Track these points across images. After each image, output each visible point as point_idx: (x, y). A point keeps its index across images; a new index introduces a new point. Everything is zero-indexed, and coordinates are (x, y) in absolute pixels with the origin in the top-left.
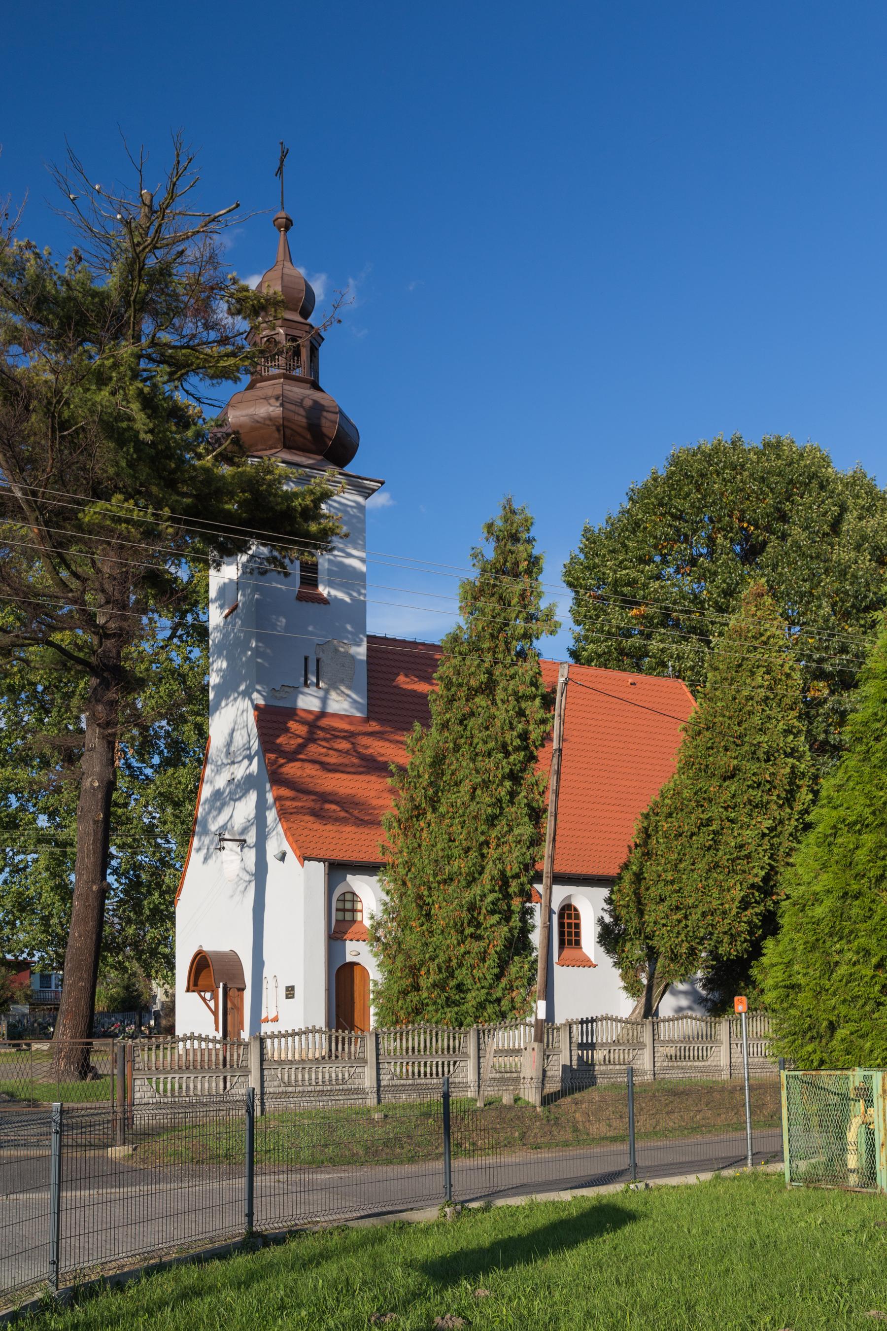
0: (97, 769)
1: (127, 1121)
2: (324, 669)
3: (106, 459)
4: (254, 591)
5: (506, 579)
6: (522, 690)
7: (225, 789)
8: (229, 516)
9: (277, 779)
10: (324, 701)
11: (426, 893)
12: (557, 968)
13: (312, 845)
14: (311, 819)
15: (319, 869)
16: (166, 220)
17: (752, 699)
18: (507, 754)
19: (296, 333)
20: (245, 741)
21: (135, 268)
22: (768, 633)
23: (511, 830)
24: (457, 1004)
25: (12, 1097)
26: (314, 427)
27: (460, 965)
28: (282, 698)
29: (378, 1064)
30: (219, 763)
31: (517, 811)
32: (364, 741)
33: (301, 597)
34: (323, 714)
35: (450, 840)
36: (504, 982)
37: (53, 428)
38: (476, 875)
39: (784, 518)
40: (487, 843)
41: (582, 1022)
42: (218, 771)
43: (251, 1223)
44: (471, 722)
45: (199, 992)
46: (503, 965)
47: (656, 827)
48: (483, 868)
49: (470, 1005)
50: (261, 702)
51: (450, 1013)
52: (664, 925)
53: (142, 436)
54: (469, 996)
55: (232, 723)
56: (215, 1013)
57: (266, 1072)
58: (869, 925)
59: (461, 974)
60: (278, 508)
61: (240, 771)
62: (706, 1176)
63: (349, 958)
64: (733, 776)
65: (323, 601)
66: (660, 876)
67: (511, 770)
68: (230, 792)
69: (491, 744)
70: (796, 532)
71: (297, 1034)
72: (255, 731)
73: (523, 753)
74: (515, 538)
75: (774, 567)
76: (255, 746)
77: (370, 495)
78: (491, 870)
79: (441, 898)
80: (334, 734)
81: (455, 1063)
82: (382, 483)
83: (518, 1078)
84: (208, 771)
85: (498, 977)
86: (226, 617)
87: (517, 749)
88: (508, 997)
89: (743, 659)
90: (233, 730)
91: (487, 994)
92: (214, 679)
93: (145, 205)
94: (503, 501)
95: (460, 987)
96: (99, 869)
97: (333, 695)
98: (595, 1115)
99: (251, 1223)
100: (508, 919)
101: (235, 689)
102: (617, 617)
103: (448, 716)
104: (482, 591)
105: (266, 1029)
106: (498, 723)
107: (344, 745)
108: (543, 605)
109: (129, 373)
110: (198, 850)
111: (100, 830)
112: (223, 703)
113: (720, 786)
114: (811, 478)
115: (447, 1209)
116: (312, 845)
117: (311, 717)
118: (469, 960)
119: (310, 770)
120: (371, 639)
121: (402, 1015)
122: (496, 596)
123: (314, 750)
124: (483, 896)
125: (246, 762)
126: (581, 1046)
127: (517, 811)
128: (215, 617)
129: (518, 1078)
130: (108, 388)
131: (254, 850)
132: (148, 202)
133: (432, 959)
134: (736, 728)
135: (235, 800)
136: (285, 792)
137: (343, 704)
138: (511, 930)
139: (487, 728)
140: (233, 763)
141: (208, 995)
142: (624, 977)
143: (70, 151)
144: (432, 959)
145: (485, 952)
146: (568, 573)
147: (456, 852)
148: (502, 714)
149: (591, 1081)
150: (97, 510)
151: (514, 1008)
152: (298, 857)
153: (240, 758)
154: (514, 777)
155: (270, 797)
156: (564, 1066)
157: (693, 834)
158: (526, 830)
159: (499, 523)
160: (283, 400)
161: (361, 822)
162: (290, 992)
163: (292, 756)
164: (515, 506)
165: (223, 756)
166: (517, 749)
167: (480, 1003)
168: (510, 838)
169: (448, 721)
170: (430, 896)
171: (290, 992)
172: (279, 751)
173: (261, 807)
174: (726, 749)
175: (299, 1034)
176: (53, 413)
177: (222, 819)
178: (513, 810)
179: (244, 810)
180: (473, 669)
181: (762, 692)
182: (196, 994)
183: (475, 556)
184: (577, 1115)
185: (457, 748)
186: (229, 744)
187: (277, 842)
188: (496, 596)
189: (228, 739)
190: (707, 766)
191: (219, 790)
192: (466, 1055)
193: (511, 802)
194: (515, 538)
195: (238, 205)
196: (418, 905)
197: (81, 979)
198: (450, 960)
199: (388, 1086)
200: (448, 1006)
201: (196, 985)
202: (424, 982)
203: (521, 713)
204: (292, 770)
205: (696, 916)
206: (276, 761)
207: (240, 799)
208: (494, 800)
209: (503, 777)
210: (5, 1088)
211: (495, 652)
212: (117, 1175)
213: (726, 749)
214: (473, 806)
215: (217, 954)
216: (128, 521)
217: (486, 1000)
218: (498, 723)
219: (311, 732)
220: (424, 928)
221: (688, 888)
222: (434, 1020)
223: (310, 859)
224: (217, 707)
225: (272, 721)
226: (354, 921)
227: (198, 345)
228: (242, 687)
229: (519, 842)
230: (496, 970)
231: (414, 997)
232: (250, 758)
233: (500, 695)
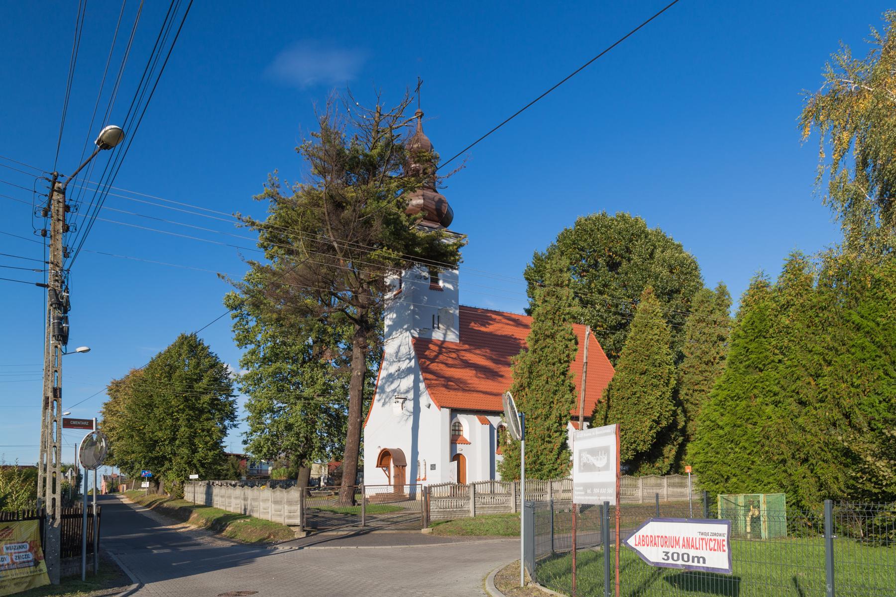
4: (413, 284)
8: (417, 254)
9: (425, 370)
10: (445, 335)
12: (496, 455)
15: (446, 412)
24: (539, 470)
26: (439, 211)
32: (463, 353)
33: (432, 288)
34: (444, 342)
36: (559, 461)
39: (628, 250)
40: (553, 402)
42: (391, 363)
46: (559, 454)
49: (545, 471)
50: (417, 335)
55: (399, 344)
56: (389, 477)
58: (745, 437)
59: (542, 458)
61: (404, 365)
63: (458, 452)
64: (645, 373)
65: (441, 290)
70: (635, 258)
72: (412, 348)
75: (626, 274)
76: (413, 354)
78: (555, 414)
80: (450, 350)
84: (384, 364)
85: (556, 459)
95: (541, 464)
97: (449, 333)
101: (401, 327)
107: (454, 355)
110: (379, 400)
114: (635, 234)
117: (439, 343)
118: (545, 452)
119: (442, 366)
120: (461, 308)
123: (441, 357)
125: (408, 361)
137: (452, 337)
146: (525, 274)
147: (539, 406)
148: (560, 348)
154: (564, 374)
155: (421, 377)
161: (464, 390)
162: (433, 467)
163: (433, 360)
168: (563, 400)
172: (426, 357)
175: (440, 486)
177: (393, 386)
179: (408, 382)
181: (657, 337)
186: (397, 353)
204: (434, 366)
205: (630, 434)
212: (424, 540)
214: (547, 386)
215: (393, 450)
219: (440, 350)
225: (421, 345)
226: (459, 435)
228: (405, 327)
232: (410, 360)
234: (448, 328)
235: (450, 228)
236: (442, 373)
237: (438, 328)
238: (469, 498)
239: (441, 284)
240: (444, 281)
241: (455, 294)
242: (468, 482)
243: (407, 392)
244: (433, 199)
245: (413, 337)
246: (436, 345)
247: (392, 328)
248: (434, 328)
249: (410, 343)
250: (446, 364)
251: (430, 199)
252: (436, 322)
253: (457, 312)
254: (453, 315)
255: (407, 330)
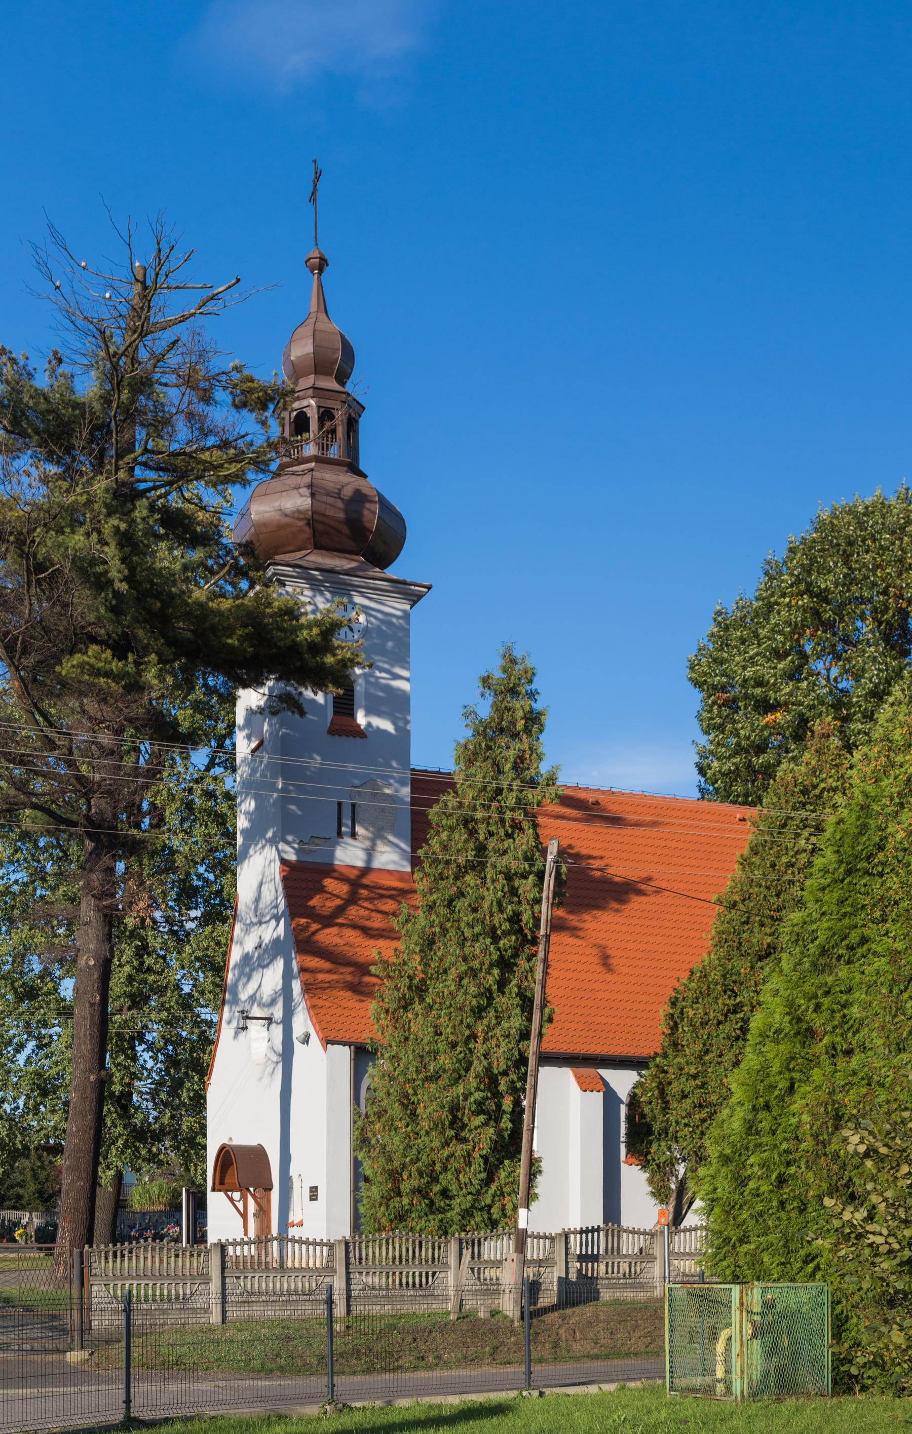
0: (92, 946)
1: (85, 1328)
2: (359, 815)
3: (87, 607)
5: (503, 741)
6: (514, 865)
7: (253, 953)
10: (370, 853)
11: (410, 1091)
13: (338, 1026)
14: (349, 994)
15: (344, 1054)
16: (152, 311)
17: (793, 865)
18: (496, 939)
19: (329, 404)
20: (273, 897)
21: (114, 378)
22: (823, 785)
23: (499, 1024)
25: (8, 1301)
27: (445, 1169)
28: (311, 851)
29: (348, 1273)
30: (248, 921)
31: (507, 1001)
33: (333, 731)
34: (366, 871)
35: (436, 1034)
36: (494, 1187)
37: (28, 571)
38: (463, 1073)
41: (581, 1232)
43: (128, 1408)
44: (459, 904)
45: (226, 1191)
47: (682, 1013)
48: (470, 1063)
50: (292, 857)
51: (433, 1222)
52: (686, 1125)
53: (117, 585)
54: (454, 1203)
55: (258, 876)
56: (244, 1216)
57: (227, 1280)
59: (447, 1179)
60: (282, 644)
62: (611, 1387)
64: (768, 955)
65: (359, 733)
66: (681, 1069)
67: (501, 956)
68: (259, 958)
69: (477, 929)
71: (297, 1241)
72: (280, 889)
73: (513, 938)
74: (513, 692)
77: (420, 596)
78: (478, 1067)
79: (426, 1097)
80: (380, 893)
81: (434, 1274)
82: (429, 588)
83: (498, 1290)
86: (253, 751)
87: (506, 933)
88: (498, 1204)
89: (788, 818)
90: (261, 885)
91: (475, 1200)
92: (242, 823)
93: (137, 280)
94: (502, 650)
95: (445, 1193)
96: (96, 1057)
97: (381, 847)
98: (581, 1331)
99: (128, 1408)
100: (498, 1120)
102: (748, 726)
103: (435, 896)
104: (475, 754)
105: (293, 1232)
106: (486, 905)
108: (544, 768)
109: (104, 510)
111: (97, 1014)
112: (251, 852)
113: (752, 968)
115: (328, 1407)
116: (338, 1026)
117: (353, 874)
118: (454, 1164)
119: (351, 935)
121: (384, 1221)
122: (490, 761)
123: (354, 912)
124: (466, 1097)
125: (273, 923)
126: (581, 1258)
127: (507, 1001)
128: (243, 746)
129: (498, 1290)
130: (82, 530)
131: (281, 1027)
132: (140, 278)
133: (413, 1162)
134: (773, 900)
135: (264, 967)
136: (313, 962)
137: (390, 858)
138: (499, 1132)
139: (475, 910)
140: (260, 923)
141: (236, 1195)
142: (651, 1181)
143: (51, 226)
144: (413, 1162)
145: (469, 1155)
149: (594, 1296)
150: (75, 662)
151: (505, 1216)
152: (321, 1040)
153: (268, 918)
154: (505, 965)
155: (295, 966)
156: (560, 1278)
157: (719, 1023)
158: (516, 1022)
159: (498, 674)
160: (314, 490)
162: (314, 1193)
163: (327, 921)
164: (518, 654)
165: (251, 913)
166: (506, 933)
167: (467, 1210)
169: (434, 902)
170: (416, 1094)
171: (314, 1193)
173: (287, 977)
174: (762, 925)
176: (27, 555)
178: (503, 1000)
179: (271, 978)
180: (460, 846)
182: (222, 1194)
183: (466, 715)
184: (562, 1331)
185: (444, 931)
186: (257, 900)
187: (302, 1022)
188: (490, 761)
189: (256, 894)
190: (740, 943)
191: (248, 954)
192: (447, 1266)
193: (501, 990)
194: (513, 692)
195: (238, 280)
196: (402, 1104)
197: (79, 1178)
198: (434, 1163)
199: (359, 1296)
200: (432, 1213)
201: (222, 1183)
202: (405, 1187)
203: (514, 892)
204: (328, 937)
206: (308, 926)
207: (267, 965)
208: (482, 990)
209: (492, 965)
210: (4, 1295)
211: (488, 824)
213: (762, 925)
216: (108, 674)
217: (472, 1207)
218: (486, 905)
220: (409, 1129)
221: (713, 1084)
222: (418, 1228)
223: (333, 1043)
224: (245, 855)
225: (302, 882)
227: (195, 452)
228: (270, 834)
229: (508, 1036)
230: (483, 1175)
231: (395, 1203)
232: (277, 918)
233: (490, 873)
234: (378, 835)
235: (392, 572)
236: (349, 953)
237: (353, 835)
238: (205, 1278)
239: (361, 719)
240: (369, 712)
241: (400, 743)
242: (212, 1239)
243: (273, 1002)
244: (338, 495)
245: (283, 861)
246: (343, 879)
247: (252, 836)
248: (340, 834)
249: (278, 878)
250: (366, 931)
251: (328, 494)
252: (347, 821)
253: (406, 792)
254: (393, 799)
255: (273, 842)
